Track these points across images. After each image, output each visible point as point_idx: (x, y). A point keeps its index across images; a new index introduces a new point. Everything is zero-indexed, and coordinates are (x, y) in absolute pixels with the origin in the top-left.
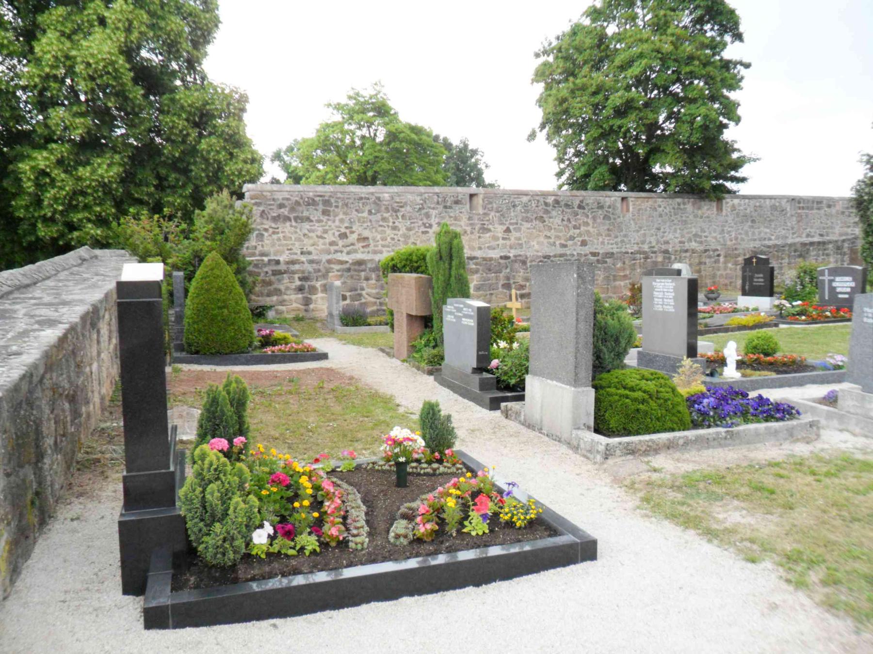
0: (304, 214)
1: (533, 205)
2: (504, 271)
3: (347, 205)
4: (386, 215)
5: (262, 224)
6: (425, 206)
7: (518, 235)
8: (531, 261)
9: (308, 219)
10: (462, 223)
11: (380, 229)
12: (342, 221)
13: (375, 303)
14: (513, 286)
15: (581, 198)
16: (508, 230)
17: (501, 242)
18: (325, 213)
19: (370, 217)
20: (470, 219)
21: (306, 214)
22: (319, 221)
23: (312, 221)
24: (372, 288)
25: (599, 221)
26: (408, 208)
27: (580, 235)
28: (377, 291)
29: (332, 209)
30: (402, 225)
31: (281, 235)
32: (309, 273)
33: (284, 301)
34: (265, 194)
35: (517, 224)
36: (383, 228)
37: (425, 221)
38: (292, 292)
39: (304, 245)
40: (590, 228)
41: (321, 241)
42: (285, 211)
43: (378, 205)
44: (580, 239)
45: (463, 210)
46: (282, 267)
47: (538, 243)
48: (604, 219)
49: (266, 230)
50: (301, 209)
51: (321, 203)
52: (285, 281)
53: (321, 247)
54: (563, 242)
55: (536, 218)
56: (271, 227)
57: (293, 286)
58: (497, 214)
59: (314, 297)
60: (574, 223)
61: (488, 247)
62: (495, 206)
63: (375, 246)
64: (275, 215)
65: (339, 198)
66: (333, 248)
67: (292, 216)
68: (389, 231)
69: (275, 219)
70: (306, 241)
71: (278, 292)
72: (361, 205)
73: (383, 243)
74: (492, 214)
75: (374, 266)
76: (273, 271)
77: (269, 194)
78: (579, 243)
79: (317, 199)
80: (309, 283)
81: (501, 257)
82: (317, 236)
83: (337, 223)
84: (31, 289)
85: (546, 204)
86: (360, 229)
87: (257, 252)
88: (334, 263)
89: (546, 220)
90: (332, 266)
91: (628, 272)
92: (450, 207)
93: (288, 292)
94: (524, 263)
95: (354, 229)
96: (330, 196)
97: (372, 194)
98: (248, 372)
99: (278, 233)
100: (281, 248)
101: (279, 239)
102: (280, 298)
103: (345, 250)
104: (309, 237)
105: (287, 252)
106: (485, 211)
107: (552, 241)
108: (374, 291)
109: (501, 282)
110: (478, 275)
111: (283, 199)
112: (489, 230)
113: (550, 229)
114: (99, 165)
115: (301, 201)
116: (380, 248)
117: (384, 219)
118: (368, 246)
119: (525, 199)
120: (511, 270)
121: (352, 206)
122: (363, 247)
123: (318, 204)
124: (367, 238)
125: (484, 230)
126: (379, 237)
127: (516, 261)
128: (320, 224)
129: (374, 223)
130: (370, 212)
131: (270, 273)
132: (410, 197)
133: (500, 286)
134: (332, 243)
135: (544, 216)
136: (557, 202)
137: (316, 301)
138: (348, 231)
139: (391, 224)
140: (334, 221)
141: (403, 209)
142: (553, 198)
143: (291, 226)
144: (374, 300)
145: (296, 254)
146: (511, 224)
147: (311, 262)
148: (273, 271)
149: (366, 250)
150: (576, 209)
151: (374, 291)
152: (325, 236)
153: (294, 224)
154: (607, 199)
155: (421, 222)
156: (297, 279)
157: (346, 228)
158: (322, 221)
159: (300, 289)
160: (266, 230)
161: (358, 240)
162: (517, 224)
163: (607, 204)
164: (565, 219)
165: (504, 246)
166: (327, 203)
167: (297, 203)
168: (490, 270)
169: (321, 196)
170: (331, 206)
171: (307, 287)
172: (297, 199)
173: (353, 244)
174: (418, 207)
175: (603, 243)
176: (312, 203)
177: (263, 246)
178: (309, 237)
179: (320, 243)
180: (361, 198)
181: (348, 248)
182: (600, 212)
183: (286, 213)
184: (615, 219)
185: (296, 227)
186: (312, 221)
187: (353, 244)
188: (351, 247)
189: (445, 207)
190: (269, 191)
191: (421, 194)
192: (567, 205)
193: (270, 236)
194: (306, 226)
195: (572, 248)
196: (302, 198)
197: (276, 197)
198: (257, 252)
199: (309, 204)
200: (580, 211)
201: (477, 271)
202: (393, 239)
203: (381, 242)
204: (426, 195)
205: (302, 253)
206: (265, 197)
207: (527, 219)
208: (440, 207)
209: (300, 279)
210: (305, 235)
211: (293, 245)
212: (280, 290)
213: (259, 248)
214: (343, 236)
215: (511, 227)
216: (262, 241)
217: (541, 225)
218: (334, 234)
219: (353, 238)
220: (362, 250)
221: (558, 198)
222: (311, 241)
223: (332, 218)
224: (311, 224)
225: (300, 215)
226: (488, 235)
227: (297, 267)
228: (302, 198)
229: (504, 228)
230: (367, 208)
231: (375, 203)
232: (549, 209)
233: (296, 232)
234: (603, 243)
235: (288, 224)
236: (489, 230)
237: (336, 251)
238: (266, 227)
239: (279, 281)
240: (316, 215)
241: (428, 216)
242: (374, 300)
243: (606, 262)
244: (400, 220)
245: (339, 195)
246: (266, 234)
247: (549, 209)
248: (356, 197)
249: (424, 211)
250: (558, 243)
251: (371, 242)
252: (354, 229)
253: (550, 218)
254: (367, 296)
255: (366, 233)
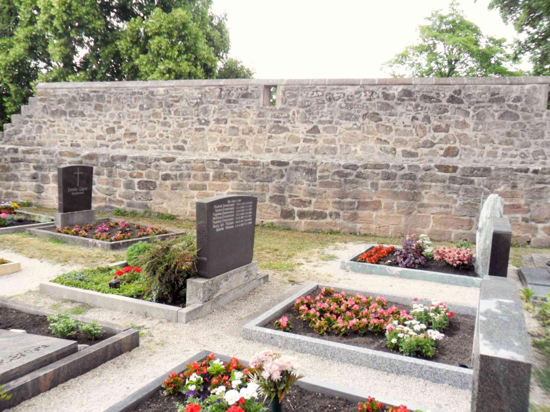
0: (79, 109)
1: (363, 98)
2: (276, 180)
3: (119, 100)
4: (159, 110)
5: (43, 117)
6: (204, 100)
7: (330, 136)
8: (323, 171)
9: (82, 114)
10: (248, 120)
11: (151, 124)
12: (112, 116)
13: (105, 199)
14: (289, 200)
15: (457, 87)
16: (315, 130)
17: (301, 144)
18: (98, 108)
19: (142, 112)
20: (260, 115)
21: (80, 109)
22: (91, 116)
23: (84, 116)
24: (103, 184)
25: (489, 120)
26: (183, 103)
27: (446, 140)
28: (108, 187)
29: (104, 104)
30: (172, 119)
31: (56, 128)
32: (43, 163)
33: (19, 186)
34: (48, 90)
35: (330, 122)
36: (153, 124)
37: (201, 116)
38: (26, 179)
39: (75, 138)
40: (470, 132)
41: (90, 134)
42: (62, 107)
43: (151, 99)
44: (445, 146)
45: (253, 105)
46: (20, 156)
47: (363, 148)
48: (502, 117)
49: (45, 123)
50: (76, 104)
51: (95, 98)
52: (22, 169)
53: (89, 140)
54: (409, 149)
55: (365, 116)
56: (49, 121)
57: (28, 174)
58: (301, 110)
59: (46, 186)
60: (436, 123)
61: (281, 150)
62: (300, 99)
63: (141, 142)
64: (54, 109)
65: (111, 94)
66: (99, 142)
67: (68, 111)
68: (158, 127)
69: (53, 113)
70: (77, 134)
71: (14, 178)
72: (133, 100)
73: (151, 139)
74: (294, 109)
75: (106, 161)
76: (11, 158)
77: (52, 91)
78: (442, 152)
79: (92, 94)
80: (43, 172)
81: (273, 163)
82: (87, 131)
83: (107, 118)
84: (185, 160)
85: (386, 96)
86: (128, 124)
87: (35, 142)
88: (65, 155)
89: (383, 117)
90: (64, 158)
91: (522, 202)
92: (235, 102)
93: (24, 179)
94: (311, 172)
95: (122, 124)
96: (104, 92)
97: (147, 88)
98: (348, 352)
99: (54, 126)
100: (55, 139)
101: (54, 132)
102: (17, 183)
103: (111, 144)
104: (79, 131)
105: (59, 143)
106: (284, 106)
107: (389, 147)
108: (105, 187)
109: (270, 194)
110: (235, 182)
111: (62, 95)
112: (286, 129)
113: (388, 130)
114: (48, 36)
115: (78, 97)
116: (146, 144)
117: (155, 115)
118: (134, 141)
119: (350, 90)
120: (288, 179)
121: (124, 101)
122: (129, 142)
123: (92, 100)
124: (135, 134)
125: (278, 128)
126: (147, 132)
127: (296, 169)
128: (91, 118)
129: (144, 118)
130: (141, 108)
131: (9, 160)
132: (187, 90)
133: (267, 197)
134: (99, 137)
135: (381, 112)
136: (408, 94)
137: (47, 189)
138: (116, 126)
139: (162, 120)
140: (105, 116)
141: (178, 104)
142: (400, 88)
143: (66, 120)
144: (105, 196)
145: (67, 146)
146: (320, 122)
147: (45, 153)
148: (11, 158)
149: (131, 145)
150: (444, 102)
151: (105, 187)
152: (94, 130)
153: (68, 118)
154: (515, 87)
155: (196, 118)
156: (32, 167)
157: (115, 123)
158: (94, 116)
159: (34, 177)
160: (45, 123)
161: (125, 135)
162: (330, 122)
163: (514, 95)
164: (420, 116)
165: (306, 151)
166: (100, 98)
167: (74, 99)
168: (253, 177)
169: (95, 92)
170: (104, 102)
171: (40, 175)
172: (74, 95)
173: (119, 139)
174: (195, 101)
175: (493, 154)
176: (86, 98)
177: (40, 137)
178: (79, 131)
179: (89, 137)
180: (134, 93)
181: (114, 143)
182: (495, 107)
183: (63, 108)
184: (526, 118)
185: (70, 121)
186: (84, 116)
187: (119, 139)
188: (117, 142)
189: (229, 101)
190: (52, 89)
191: (201, 87)
192: (426, 98)
193: (48, 128)
194: (79, 120)
195: (427, 158)
196: (78, 94)
197: (57, 93)
198: (35, 142)
199: (84, 100)
200: (452, 106)
201: (234, 177)
202: (161, 135)
203: (148, 138)
204: (207, 89)
205: (72, 145)
206: (49, 93)
207: (348, 117)
208: (223, 102)
209: (35, 168)
210: (76, 128)
211: (66, 137)
212: (16, 176)
213: (38, 139)
214: (111, 130)
215: (320, 127)
216: (41, 133)
217: (373, 124)
218: (102, 128)
219: (120, 132)
220: (127, 145)
221: (410, 88)
222: (81, 135)
223: (104, 113)
224: (83, 118)
225: (76, 110)
226: (283, 135)
227: (32, 156)
228: (78, 94)
229: (310, 127)
230: (140, 103)
231: (148, 97)
232: (391, 103)
233: (69, 126)
234: (493, 154)
235: (63, 118)
236: (286, 129)
237: (102, 145)
238: (45, 120)
239: (16, 167)
240: (89, 110)
241: (206, 111)
242: (105, 196)
243: (472, 182)
244: (173, 115)
245: (113, 90)
246: (44, 126)
247: (391, 103)
248: (129, 92)
249: (201, 107)
250: (399, 150)
251: (138, 137)
252: (122, 124)
253: (391, 115)
254: (96, 191)
255: (135, 129)
